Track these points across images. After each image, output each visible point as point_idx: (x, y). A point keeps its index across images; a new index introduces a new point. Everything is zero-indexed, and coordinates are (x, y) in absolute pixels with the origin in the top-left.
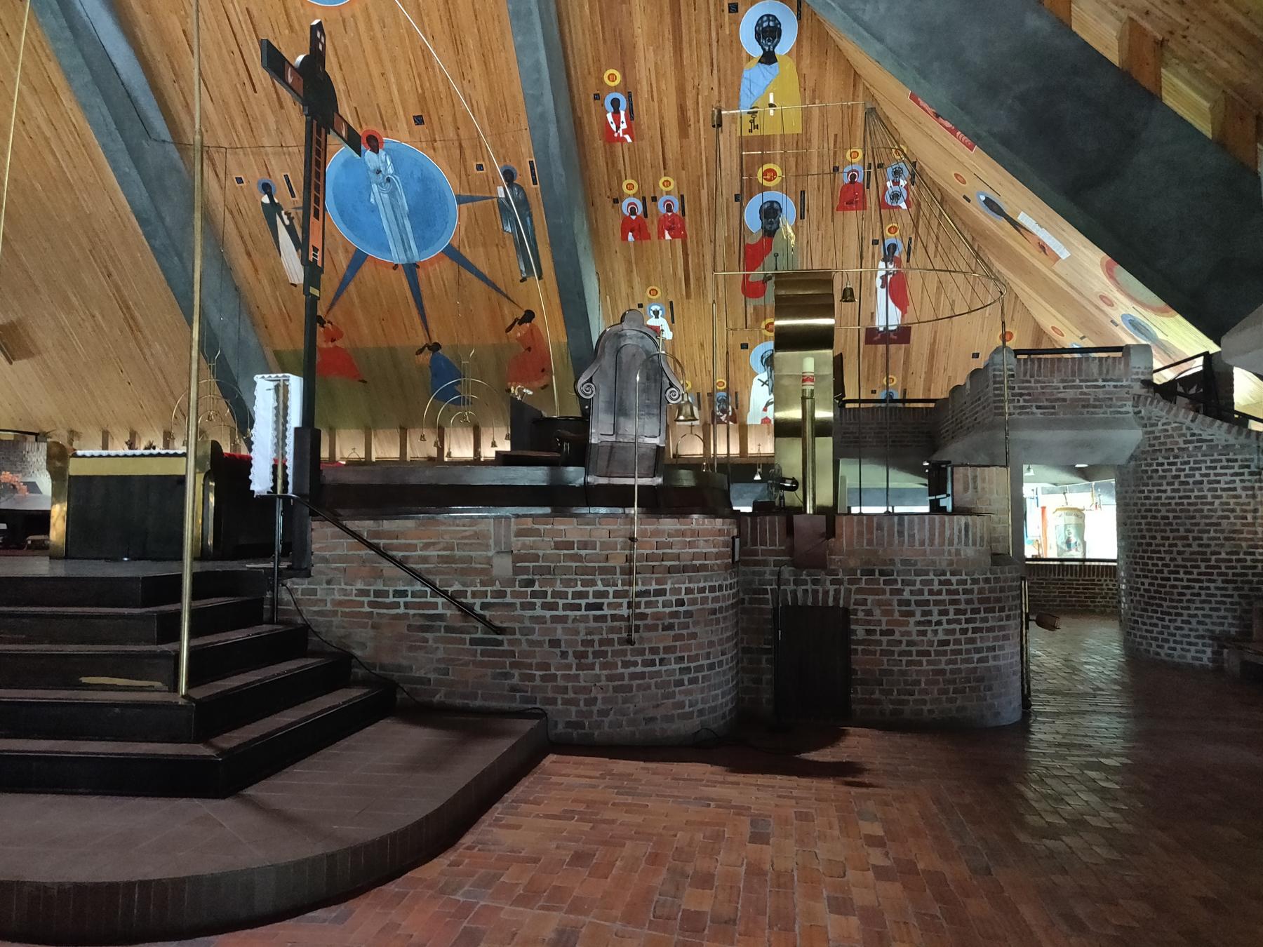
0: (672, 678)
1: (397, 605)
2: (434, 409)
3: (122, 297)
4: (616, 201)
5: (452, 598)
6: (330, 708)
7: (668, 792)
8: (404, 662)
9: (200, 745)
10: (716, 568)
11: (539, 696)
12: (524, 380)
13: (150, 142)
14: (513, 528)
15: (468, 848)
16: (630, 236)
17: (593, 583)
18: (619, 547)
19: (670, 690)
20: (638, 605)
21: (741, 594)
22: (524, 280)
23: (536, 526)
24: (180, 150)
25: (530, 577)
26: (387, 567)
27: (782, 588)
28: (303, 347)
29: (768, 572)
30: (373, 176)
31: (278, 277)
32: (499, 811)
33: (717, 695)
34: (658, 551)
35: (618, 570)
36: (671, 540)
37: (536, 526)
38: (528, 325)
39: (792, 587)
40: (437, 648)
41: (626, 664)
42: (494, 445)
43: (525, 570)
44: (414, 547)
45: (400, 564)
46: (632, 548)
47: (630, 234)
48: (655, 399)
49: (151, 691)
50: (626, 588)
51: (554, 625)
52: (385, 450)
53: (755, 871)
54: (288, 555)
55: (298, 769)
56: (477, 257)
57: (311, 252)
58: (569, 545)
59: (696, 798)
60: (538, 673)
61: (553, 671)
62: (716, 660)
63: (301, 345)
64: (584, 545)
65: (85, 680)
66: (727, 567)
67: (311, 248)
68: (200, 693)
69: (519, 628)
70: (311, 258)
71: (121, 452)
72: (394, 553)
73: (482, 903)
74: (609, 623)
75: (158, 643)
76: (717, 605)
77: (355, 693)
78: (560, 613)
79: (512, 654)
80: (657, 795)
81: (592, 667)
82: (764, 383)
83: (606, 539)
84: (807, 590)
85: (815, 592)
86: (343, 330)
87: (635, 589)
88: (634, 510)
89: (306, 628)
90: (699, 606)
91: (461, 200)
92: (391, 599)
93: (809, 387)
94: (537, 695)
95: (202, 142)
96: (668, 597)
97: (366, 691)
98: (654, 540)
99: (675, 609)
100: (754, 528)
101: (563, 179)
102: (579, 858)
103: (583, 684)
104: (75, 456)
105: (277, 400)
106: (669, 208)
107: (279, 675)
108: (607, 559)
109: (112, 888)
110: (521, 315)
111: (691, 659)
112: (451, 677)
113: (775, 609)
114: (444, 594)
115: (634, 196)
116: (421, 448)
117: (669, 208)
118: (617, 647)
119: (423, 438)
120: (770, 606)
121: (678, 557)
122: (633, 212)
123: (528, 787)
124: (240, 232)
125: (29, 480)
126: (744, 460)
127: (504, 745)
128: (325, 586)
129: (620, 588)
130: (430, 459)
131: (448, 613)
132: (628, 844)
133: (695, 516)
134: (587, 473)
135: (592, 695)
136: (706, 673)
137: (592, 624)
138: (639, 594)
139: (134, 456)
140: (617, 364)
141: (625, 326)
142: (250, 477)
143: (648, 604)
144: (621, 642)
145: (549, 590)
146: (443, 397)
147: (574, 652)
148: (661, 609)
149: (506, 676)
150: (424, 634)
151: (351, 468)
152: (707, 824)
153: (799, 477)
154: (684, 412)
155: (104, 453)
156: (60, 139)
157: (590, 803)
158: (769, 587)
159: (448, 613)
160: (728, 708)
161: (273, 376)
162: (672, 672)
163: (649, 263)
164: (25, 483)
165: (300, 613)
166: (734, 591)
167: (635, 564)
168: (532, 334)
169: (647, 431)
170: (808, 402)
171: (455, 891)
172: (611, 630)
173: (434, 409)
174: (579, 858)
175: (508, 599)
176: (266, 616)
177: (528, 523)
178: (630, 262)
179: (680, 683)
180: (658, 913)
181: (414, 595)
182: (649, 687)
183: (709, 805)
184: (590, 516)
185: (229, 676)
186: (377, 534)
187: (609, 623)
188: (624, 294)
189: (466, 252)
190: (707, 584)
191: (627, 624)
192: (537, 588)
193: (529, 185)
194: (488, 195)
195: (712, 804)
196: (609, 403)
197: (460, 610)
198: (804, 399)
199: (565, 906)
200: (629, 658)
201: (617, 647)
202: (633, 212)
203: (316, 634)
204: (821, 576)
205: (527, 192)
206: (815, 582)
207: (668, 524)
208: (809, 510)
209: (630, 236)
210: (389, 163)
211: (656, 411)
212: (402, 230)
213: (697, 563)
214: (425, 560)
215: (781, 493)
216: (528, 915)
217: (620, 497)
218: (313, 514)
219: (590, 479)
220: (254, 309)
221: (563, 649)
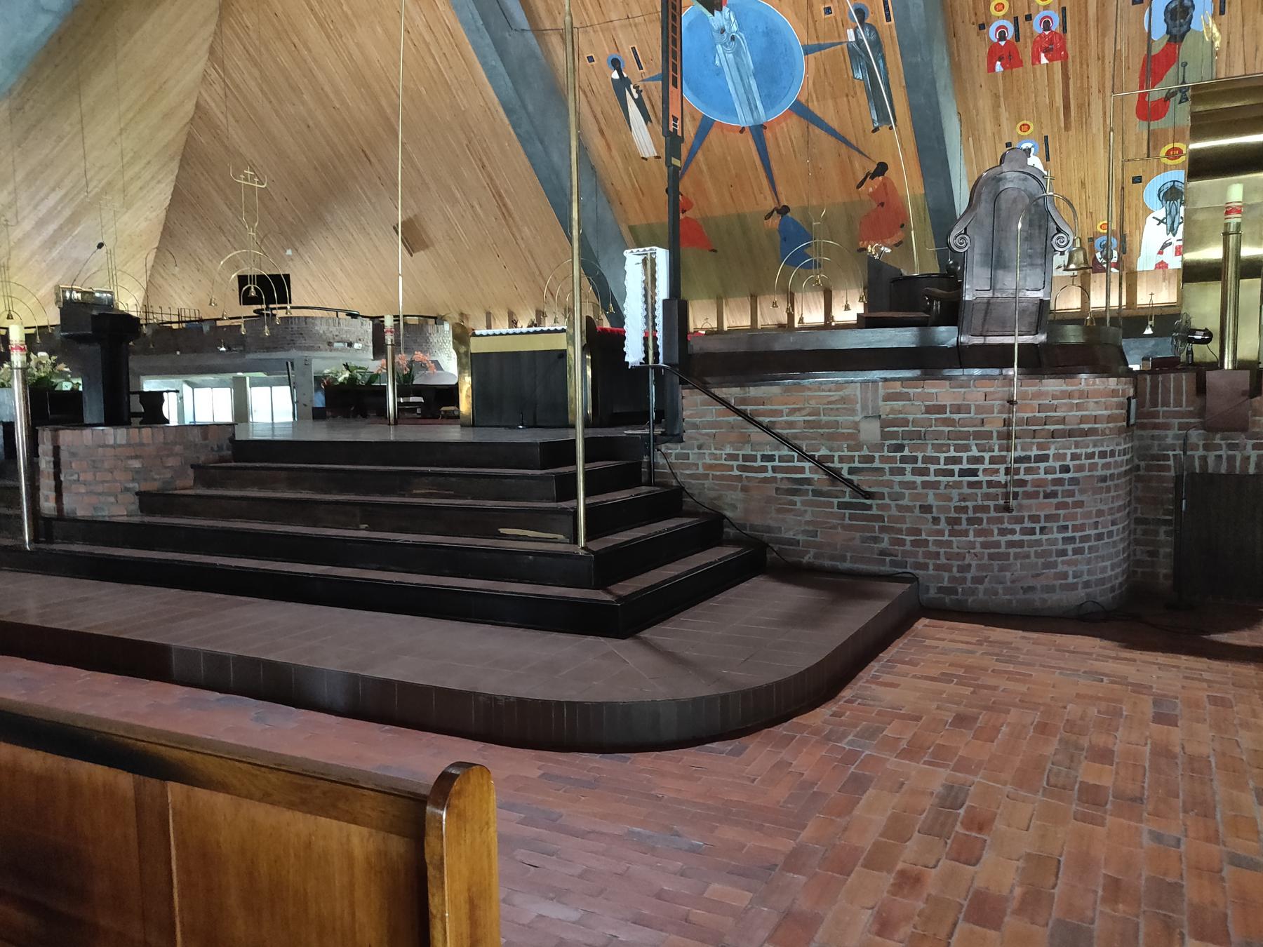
0: (1054, 547)
1: (764, 469)
2: (785, 275)
3: (495, 187)
4: (982, 27)
5: (819, 463)
6: (707, 565)
7: (1053, 663)
8: (772, 524)
9: (600, 591)
10: (1107, 432)
11: (910, 560)
12: (879, 237)
13: (513, 33)
14: (881, 392)
15: (849, 701)
16: (998, 65)
17: (967, 448)
18: (996, 411)
19: (1052, 559)
20: (1017, 471)
21: (1136, 461)
22: (876, 130)
23: (906, 390)
24: (537, 37)
25: (899, 442)
26: (754, 431)
27: (1189, 453)
28: (667, 220)
29: (1171, 436)
30: (716, 35)
31: (629, 152)
32: (876, 669)
33: (1105, 567)
34: (1040, 415)
35: (995, 435)
36: (1055, 402)
37: (906, 390)
38: (881, 178)
39: (1201, 452)
40: (806, 511)
41: (1003, 532)
42: (847, 308)
43: (894, 435)
44: (780, 413)
45: (767, 429)
46: (1010, 411)
47: (998, 63)
48: (1039, 248)
49: (555, 542)
50: (1004, 453)
51: (925, 491)
52: (736, 319)
53: (1162, 752)
54: (661, 422)
55: (681, 617)
56: (825, 110)
57: (672, 122)
58: (941, 409)
59: (1085, 672)
60: (909, 538)
61: (924, 537)
62: (1105, 530)
63: (665, 219)
64: (958, 409)
65: (502, 531)
66: (1120, 431)
67: (671, 118)
68: (597, 545)
69: (888, 493)
70: (671, 128)
71: (504, 331)
72: (760, 419)
73: (867, 752)
74: (985, 489)
75: (557, 502)
76: (1108, 472)
77: (728, 551)
78: (932, 478)
79: (881, 518)
80: (1041, 665)
81: (966, 533)
82: (1161, 221)
83: (982, 402)
84: (1220, 456)
85: (1231, 459)
86: (693, 200)
87: (1013, 454)
88: (1013, 372)
89: (680, 490)
90: (1087, 473)
91: (808, 50)
92: (759, 463)
93: (1234, 220)
94: (908, 559)
95: (572, 24)
96: (1051, 463)
97: (739, 549)
98: (1035, 403)
99: (1058, 475)
100: (1154, 387)
101: (922, 9)
102: (962, 721)
103: (956, 550)
104: (474, 335)
105: (646, 274)
106: (1047, 26)
107: (660, 532)
108: (982, 423)
109: (546, 704)
110: (872, 168)
111: (1075, 529)
112: (818, 539)
113: (1178, 479)
115: (1004, 17)
116: (771, 315)
117: (1047, 26)
118: (993, 514)
119: (775, 305)
120: (1172, 473)
121: (1063, 421)
122: (1002, 36)
123: (901, 648)
124: (593, 111)
125: (434, 359)
126: (1131, 312)
127: (877, 607)
128: (696, 451)
129: (996, 453)
130: (781, 326)
131: (816, 477)
132: (1013, 710)
133: (1084, 376)
134: (960, 333)
135: (967, 562)
136: (1093, 543)
137: (966, 490)
138: (1018, 460)
139: (515, 334)
140: (995, 211)
141: (1005, 167)
142: (625, 349)
143: (1028, 471)
144: (997, 509)
145: (920, 455)
146: (793, 262)
147: (947, 518)
148: (1042, 475)
149: (876, 540)
150: (792, 497)
151: (709, 337)
152: (1099, 698)
153: (1214, 326)
154: (1075, 259)
155: (490, 332)
156: (438, 43)
157: (969, 669)
158: (1171, 453)
159: (816, 477)
160: (1118, 581)
161: (641, 250)
162: (1055, 542)
163: (1020, 94)
164: (433, 362)
165: (675, 476)
166: (1128, 457)
167: (1014, 428)
168: (885, 188)
169: (1029, 284)
170: (1232, 239)
171: (840, 739)
172: (987, 496)
173: (785, 275)
174: (962, 721)
175: (877, 464)
176: (644, 479)
177: (897, 388)
178: (997, 96)
179: (1063, 553)
180: (1052, 780)
181: (781, 459)
182: (1027, 556)
183: (1102, 680)
184: (963, 378)
185: (618, 532)
186: (744, 401)
187: (985, 489)
188: (989, 133)
189: (815, 107)
190: (1097, 450)
191: (1004, 490)
192: (906, 452)
193: (882, 21)
194: (838, 41)
195: (1105, 679)
196: (986, 255)
197: (828, 474)
198: (1226, 234)
199: (952, 764)
200: (1006, 525)
201: (993, 514)
202: (1002, 36)
203: (690, 496)
204: (1240, 439)
205: (880, 30)
206: (1231, 447)
207: (1052, 385)
208: (1228, 364)
209: (998, 65)
210: (733, 19)
211: (1040, 261)
212: (748, 91)
213: (1086, 426)
214: (791, 425)
215: (1189, 346)
216: (914, 769)
217: (998, 357)
218: (682, 382)
219: (963, 339)
220: (609, 186)
221: (935, 514)
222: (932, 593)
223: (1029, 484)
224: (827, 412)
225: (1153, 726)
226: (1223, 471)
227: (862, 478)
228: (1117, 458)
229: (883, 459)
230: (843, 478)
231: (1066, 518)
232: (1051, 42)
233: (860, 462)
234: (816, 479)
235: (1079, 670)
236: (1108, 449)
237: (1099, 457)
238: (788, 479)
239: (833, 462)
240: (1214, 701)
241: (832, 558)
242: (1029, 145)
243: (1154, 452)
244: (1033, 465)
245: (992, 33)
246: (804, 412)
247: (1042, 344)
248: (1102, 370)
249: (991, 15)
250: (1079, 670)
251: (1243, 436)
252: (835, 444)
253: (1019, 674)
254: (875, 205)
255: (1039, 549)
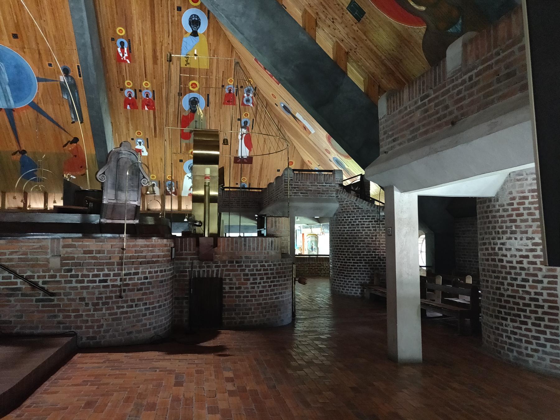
0: (141, 313)
4: (122, 90)
5: (26, 279)
10: (163, 261)
14: (61, 243)
15: (29, 407)
16: (128, 107)
17: (103, 270)
18: (116, 253)
20: (125, 280)
21: (175, 273)
22: (73, 122)
23: (74, 243)
27: (193, 270)
29: (187, 263)
35: (116, 264)
36: (142, 249)
37: (74, 243)
38: (75, 144)
39: (198, 269)
40: (17, 305)
41: (118, 308)
43: (67, 264)
46: (123, 253)
47: (128, 106)
50: (120, 272)
51: (82, 291)
53: (176, 399)
58: (91, 252)
61: (81, 313)
62: (162, 304)
64: (99, 252)
66: (168, 261)
74: (111, 289)
76: (163, 279)
82: (190, 178)
83: (110, 249)
84: (204, 270)
85: (208, 271)
88: (124, 235)
90: (155, 279)
93: (208, 181)
96: (140, 276)
98: (134, 249)
99: (143, 281)
103: (96, 318)
111: (150, 304)
113: (190, 279)
114: (22, 277)
115: (131, 88)
118: (114, 300)
119: (14, 198)
120: (188, 278)
121: (145, 257)
122: (130, 96)
126: (180, 212)
127: (51, 352)
129: (116, 272)
130: (19, 208)
131: (24, 286)
132: (115, 394)
133: (154, 238)
134: (101, 217)
135: (101, 323)
136: (157, 310)
137: (102, 289)
138: (125, 275)
140: (118, 166)
141: (122, 148)
143: (130, 279)
144: (117, 297)
145: (80, 274)
146: (27, 177)
148: (136, 281)
153: (202, 220)
154: (149, 190)
158: (187, 270)
159: (24, 286)
160: (168, 325)
162: (141, 310)
170: (207, 188)
172: (111, 292)
173: (22, 183)
175: (58, 279)
177: (70, 242)
179: (145, 315)
182: (129, 318)
184: (102, 238)
187: (111, 289)
188: (125, 133)
189: (42, 106)
190: (159, 269)
191: (119, 288)
192: (73, 273)
193: (77, 77)
196: (113, 184)
197: (30, 285)
198: (205, 186)
200: (120, 304)
204: (211, 264)
206: (208, 267)
207: (141, 242)
208: (206, 235)
209: (128, 107)
211: (136, 189)
213: (154, 259)
214: (11, 260)
217: (117, 229)
219: (102, 220)
221: (87, 302)
222: (84, 340)
223: (130, 285)
224: (32, 253)
225: (174, 388)
226: (205, 276)
227: (50, 286)
228: (167, 273)
229: (61, 276)
230: (39, 287)
231: (146, 299)
232: (149, 102)
233: (48, 278)
234: (24, 288)
235: (147, 368)
236: (163, 269)
237: (160, 273)
238: (7, 289)
239: (34, 279)
240: (198, 372)
241: (31, 328)
242: (141, 141)
243: (181, 270)
244: (132, 277)
245: (127, 95)
246: (18, 253)
247: (137, 224)
248: (162, 236)
249: (125, 86)
250: (147, 368)
251: (212, 263)
252: (36, 269)
253: (121, 374)
254: (72, 156)
255: (135, 314)
